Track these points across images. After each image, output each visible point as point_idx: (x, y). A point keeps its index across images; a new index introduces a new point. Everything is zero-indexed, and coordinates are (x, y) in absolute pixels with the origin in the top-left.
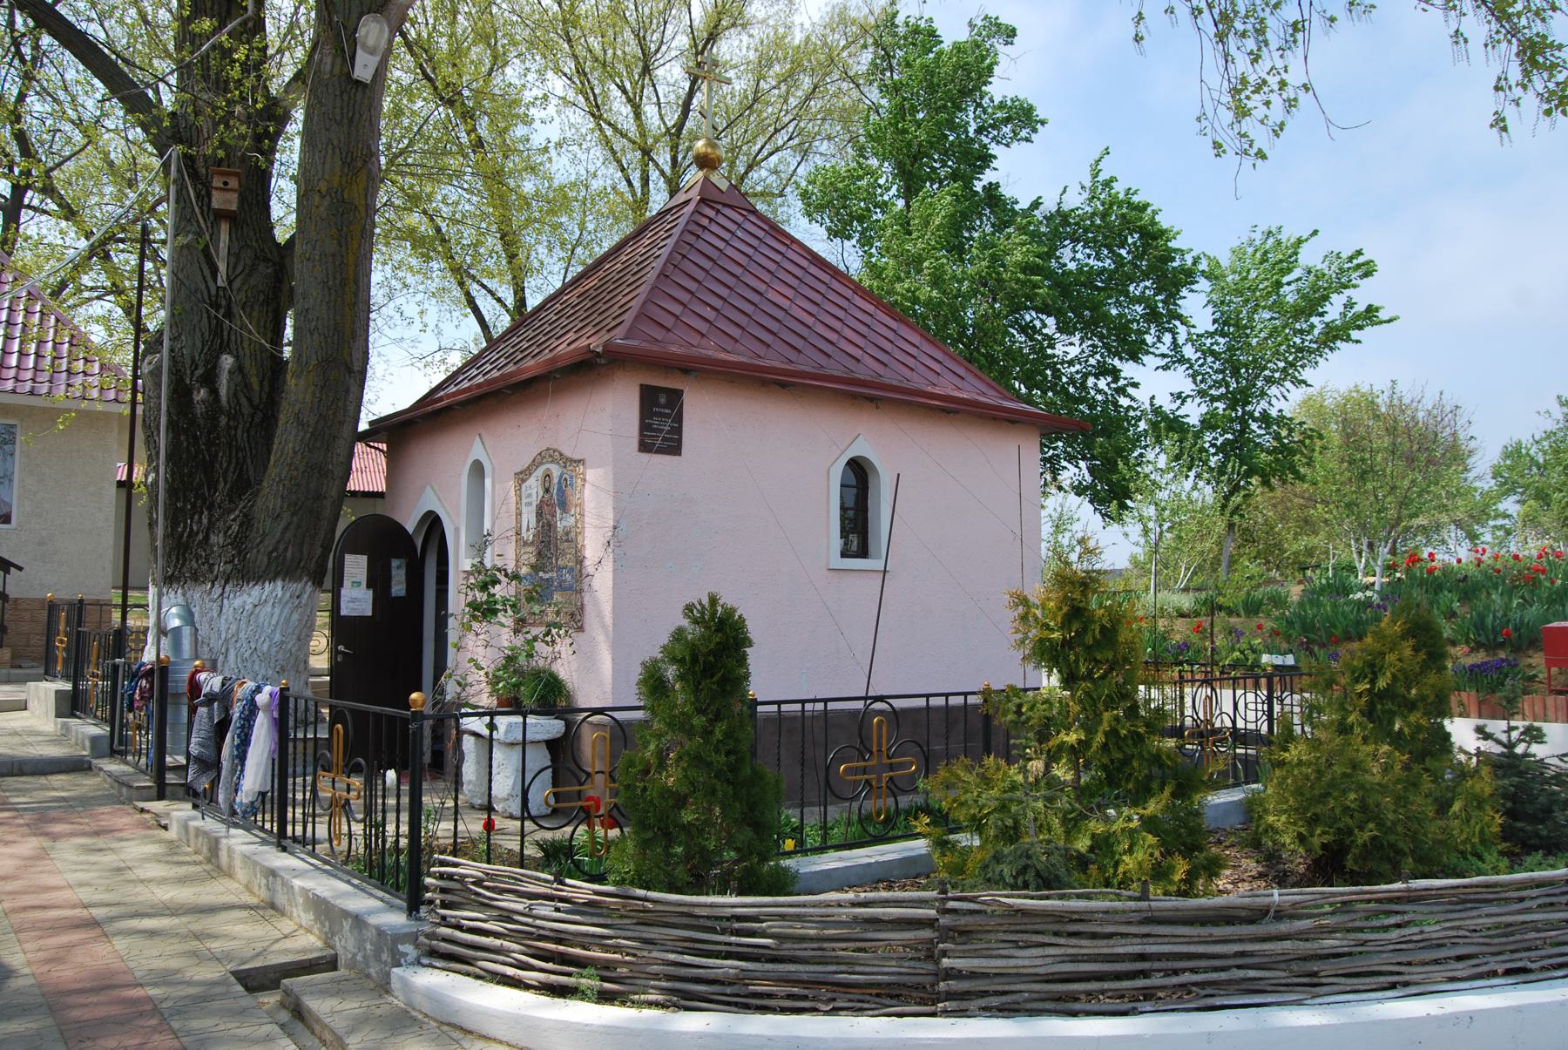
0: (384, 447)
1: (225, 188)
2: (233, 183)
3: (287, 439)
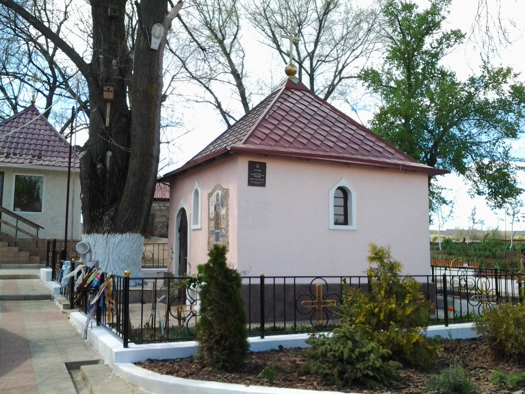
0: (169, 184)
1: (108, 90)
2: (112, 89)
3: (131, 180)
